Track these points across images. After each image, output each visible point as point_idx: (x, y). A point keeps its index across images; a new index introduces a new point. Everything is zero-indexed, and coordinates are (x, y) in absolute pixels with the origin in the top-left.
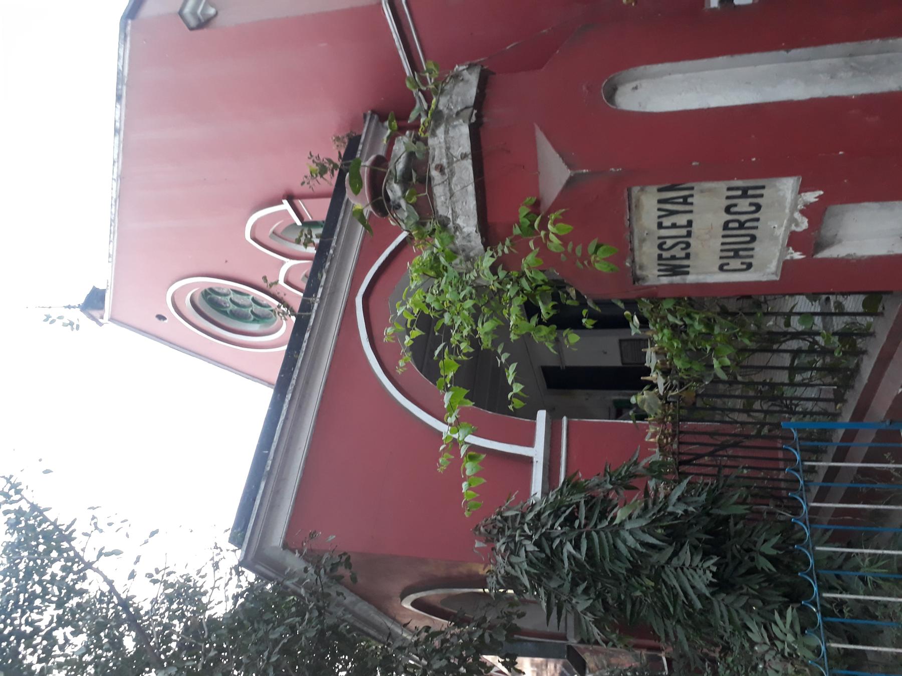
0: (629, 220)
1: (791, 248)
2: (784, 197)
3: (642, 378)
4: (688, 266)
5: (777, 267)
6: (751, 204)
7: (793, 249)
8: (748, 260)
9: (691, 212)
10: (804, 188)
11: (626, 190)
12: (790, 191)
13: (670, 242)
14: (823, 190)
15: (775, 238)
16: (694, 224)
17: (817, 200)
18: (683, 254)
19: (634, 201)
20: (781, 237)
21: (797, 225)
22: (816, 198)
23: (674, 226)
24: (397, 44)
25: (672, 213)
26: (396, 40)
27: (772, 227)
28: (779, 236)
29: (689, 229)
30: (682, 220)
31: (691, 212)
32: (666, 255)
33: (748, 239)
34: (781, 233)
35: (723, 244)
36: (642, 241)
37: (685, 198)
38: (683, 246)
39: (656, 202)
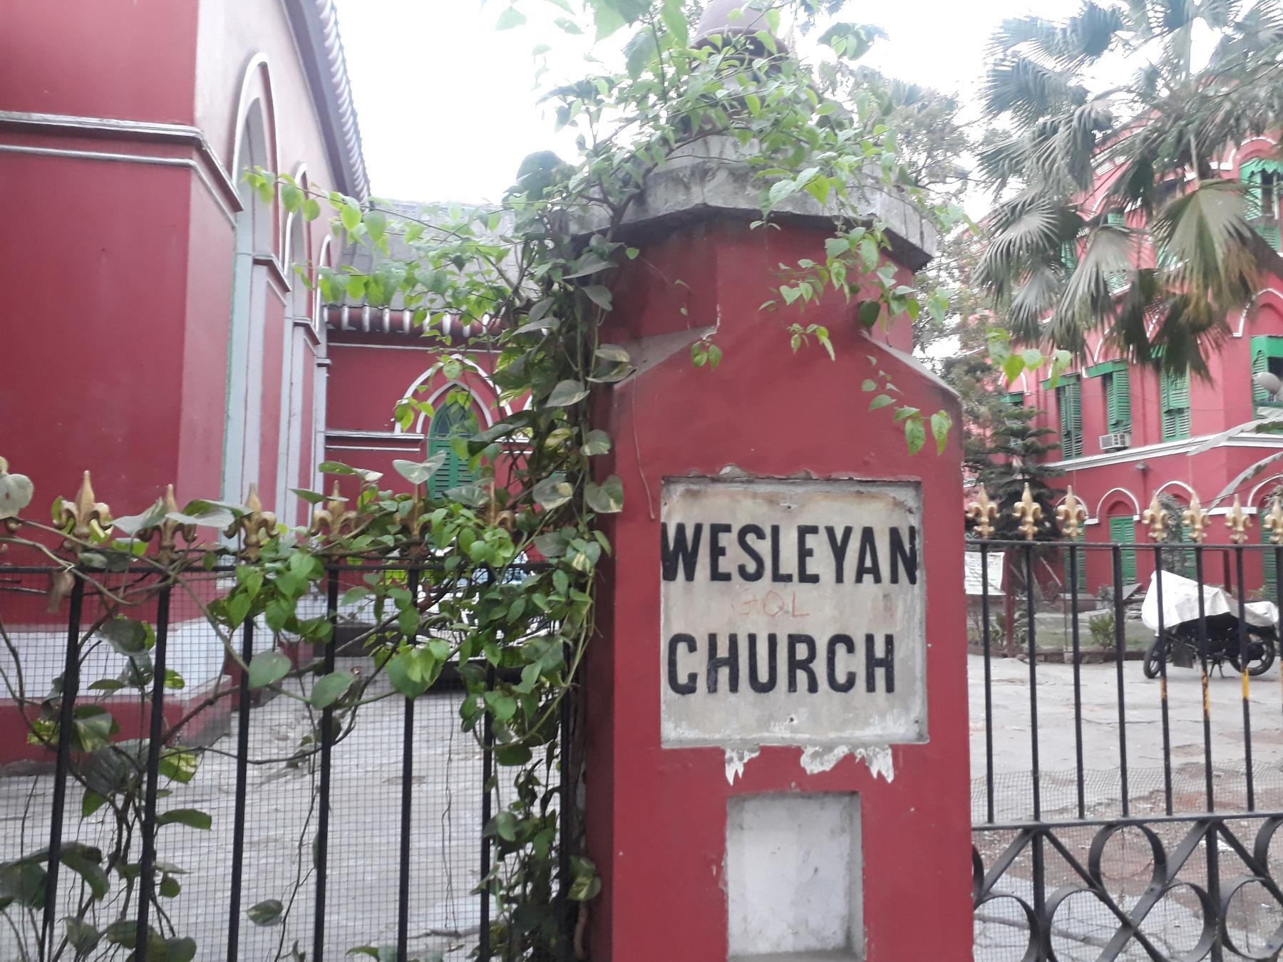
0: (851, 479)
1: (755, 755)
2: (867, 724)
3: (87, 472)
4: (690, 576)
5: (691, 741)
6: (693, 677)
7: (751, 761)
8: (702, 683)
9: (839, 579)
10: (901, 753)
11: (918, 479)
12: (880, 732)
13: (764, 547)
14: (893, 781)
15: (765, 724)
16: (807, 586)
17: (875, 775)
18: (725, 565)
19: (873, 490)
20: (766, 735)
21: (815, 755)
22: (879, 774)
23: (804, 553)
24: (114, 122)
25: (839, 552)
26: (122, 123)
27: (793, 716)
28: (769, 732)
29: (796, 577)
30: (821, 563)
31: (839, 579)
32: (728, 540)
33: (763, 676)
34: (779, 734)
35: (752, 639)
36: (771, 501)
37: (875, 571)
38: (751, 567)
39: (867, 525)
